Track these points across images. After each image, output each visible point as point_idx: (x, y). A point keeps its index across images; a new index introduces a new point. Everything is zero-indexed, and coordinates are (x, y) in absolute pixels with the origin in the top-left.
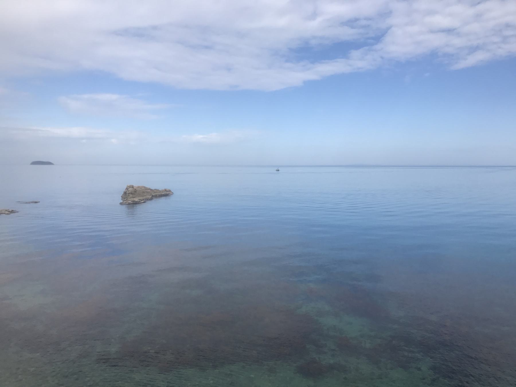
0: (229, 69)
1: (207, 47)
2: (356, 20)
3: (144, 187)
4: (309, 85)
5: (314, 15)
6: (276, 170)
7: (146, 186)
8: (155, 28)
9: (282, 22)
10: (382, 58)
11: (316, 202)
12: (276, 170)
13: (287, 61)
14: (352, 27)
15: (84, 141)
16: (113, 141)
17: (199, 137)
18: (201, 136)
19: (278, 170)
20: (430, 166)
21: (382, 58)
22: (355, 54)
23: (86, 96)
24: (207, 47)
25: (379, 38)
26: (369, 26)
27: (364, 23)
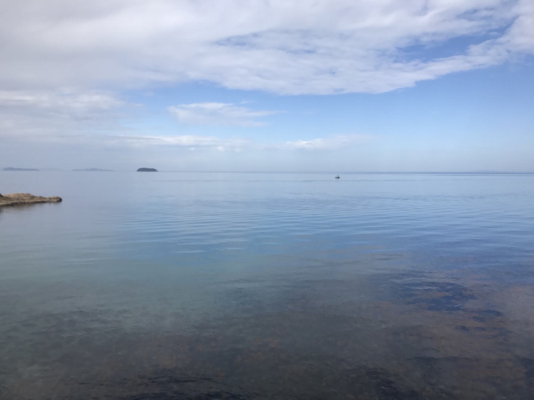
0: (333, 72)
1: (308, 52)
2: (475, 11)
3: (23, 194)
4: (421, 85)
5: (425, 9)
6: (336, 178)
7: (33, 193)
8: (255, 35)
9: (388, 20)
10: (509, 51)
11: (237, 213)
12: (336, 178)
13: (395, 61)
14: (471, 20)
15: (193, 149)
16: (220, 148)
17: (303, 143)
18: (306, 142)
19: (339, 178)
20: (468, 173)
21: (509, 51)
22: (475, 49)
23: (193, 105)
24: (308, 52)
25: (503, 30)
26: (491, 16)
27: (484, 13)
